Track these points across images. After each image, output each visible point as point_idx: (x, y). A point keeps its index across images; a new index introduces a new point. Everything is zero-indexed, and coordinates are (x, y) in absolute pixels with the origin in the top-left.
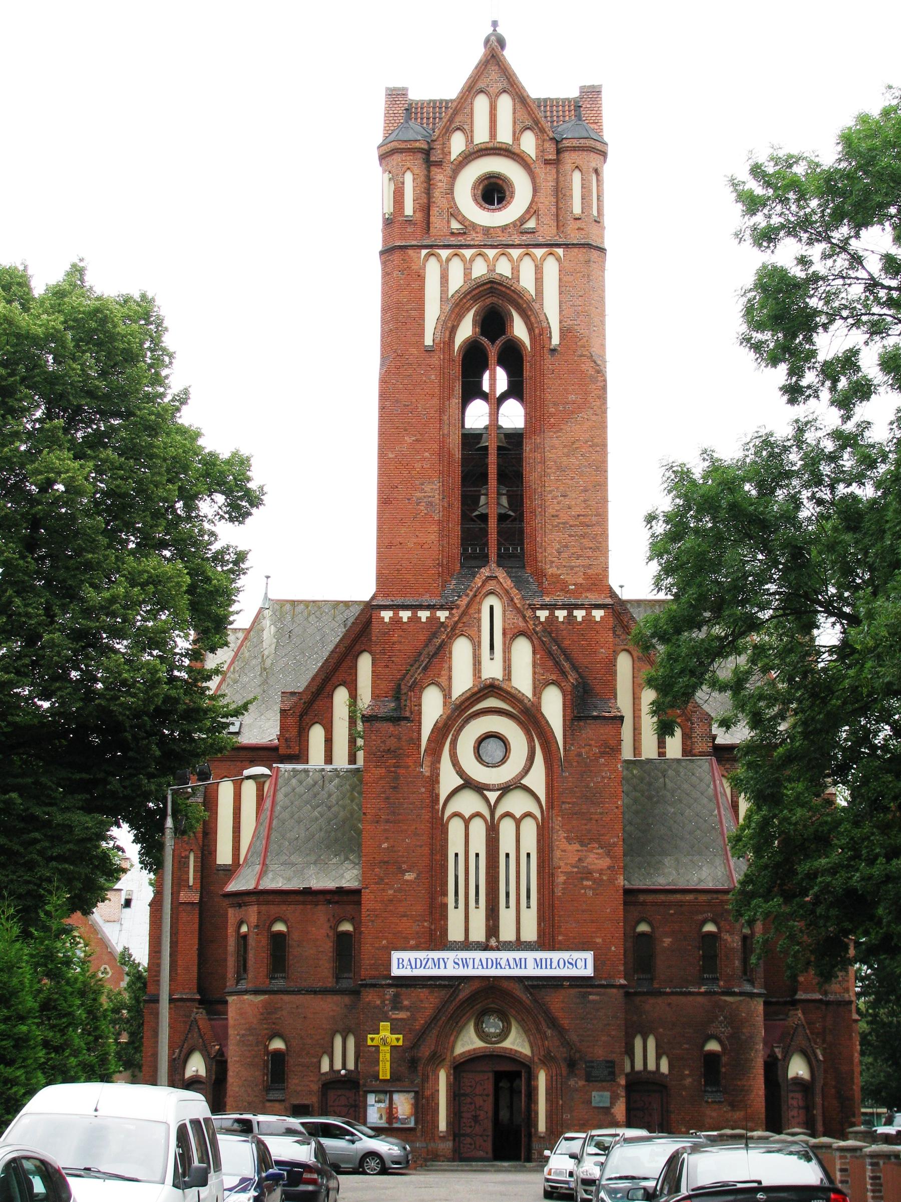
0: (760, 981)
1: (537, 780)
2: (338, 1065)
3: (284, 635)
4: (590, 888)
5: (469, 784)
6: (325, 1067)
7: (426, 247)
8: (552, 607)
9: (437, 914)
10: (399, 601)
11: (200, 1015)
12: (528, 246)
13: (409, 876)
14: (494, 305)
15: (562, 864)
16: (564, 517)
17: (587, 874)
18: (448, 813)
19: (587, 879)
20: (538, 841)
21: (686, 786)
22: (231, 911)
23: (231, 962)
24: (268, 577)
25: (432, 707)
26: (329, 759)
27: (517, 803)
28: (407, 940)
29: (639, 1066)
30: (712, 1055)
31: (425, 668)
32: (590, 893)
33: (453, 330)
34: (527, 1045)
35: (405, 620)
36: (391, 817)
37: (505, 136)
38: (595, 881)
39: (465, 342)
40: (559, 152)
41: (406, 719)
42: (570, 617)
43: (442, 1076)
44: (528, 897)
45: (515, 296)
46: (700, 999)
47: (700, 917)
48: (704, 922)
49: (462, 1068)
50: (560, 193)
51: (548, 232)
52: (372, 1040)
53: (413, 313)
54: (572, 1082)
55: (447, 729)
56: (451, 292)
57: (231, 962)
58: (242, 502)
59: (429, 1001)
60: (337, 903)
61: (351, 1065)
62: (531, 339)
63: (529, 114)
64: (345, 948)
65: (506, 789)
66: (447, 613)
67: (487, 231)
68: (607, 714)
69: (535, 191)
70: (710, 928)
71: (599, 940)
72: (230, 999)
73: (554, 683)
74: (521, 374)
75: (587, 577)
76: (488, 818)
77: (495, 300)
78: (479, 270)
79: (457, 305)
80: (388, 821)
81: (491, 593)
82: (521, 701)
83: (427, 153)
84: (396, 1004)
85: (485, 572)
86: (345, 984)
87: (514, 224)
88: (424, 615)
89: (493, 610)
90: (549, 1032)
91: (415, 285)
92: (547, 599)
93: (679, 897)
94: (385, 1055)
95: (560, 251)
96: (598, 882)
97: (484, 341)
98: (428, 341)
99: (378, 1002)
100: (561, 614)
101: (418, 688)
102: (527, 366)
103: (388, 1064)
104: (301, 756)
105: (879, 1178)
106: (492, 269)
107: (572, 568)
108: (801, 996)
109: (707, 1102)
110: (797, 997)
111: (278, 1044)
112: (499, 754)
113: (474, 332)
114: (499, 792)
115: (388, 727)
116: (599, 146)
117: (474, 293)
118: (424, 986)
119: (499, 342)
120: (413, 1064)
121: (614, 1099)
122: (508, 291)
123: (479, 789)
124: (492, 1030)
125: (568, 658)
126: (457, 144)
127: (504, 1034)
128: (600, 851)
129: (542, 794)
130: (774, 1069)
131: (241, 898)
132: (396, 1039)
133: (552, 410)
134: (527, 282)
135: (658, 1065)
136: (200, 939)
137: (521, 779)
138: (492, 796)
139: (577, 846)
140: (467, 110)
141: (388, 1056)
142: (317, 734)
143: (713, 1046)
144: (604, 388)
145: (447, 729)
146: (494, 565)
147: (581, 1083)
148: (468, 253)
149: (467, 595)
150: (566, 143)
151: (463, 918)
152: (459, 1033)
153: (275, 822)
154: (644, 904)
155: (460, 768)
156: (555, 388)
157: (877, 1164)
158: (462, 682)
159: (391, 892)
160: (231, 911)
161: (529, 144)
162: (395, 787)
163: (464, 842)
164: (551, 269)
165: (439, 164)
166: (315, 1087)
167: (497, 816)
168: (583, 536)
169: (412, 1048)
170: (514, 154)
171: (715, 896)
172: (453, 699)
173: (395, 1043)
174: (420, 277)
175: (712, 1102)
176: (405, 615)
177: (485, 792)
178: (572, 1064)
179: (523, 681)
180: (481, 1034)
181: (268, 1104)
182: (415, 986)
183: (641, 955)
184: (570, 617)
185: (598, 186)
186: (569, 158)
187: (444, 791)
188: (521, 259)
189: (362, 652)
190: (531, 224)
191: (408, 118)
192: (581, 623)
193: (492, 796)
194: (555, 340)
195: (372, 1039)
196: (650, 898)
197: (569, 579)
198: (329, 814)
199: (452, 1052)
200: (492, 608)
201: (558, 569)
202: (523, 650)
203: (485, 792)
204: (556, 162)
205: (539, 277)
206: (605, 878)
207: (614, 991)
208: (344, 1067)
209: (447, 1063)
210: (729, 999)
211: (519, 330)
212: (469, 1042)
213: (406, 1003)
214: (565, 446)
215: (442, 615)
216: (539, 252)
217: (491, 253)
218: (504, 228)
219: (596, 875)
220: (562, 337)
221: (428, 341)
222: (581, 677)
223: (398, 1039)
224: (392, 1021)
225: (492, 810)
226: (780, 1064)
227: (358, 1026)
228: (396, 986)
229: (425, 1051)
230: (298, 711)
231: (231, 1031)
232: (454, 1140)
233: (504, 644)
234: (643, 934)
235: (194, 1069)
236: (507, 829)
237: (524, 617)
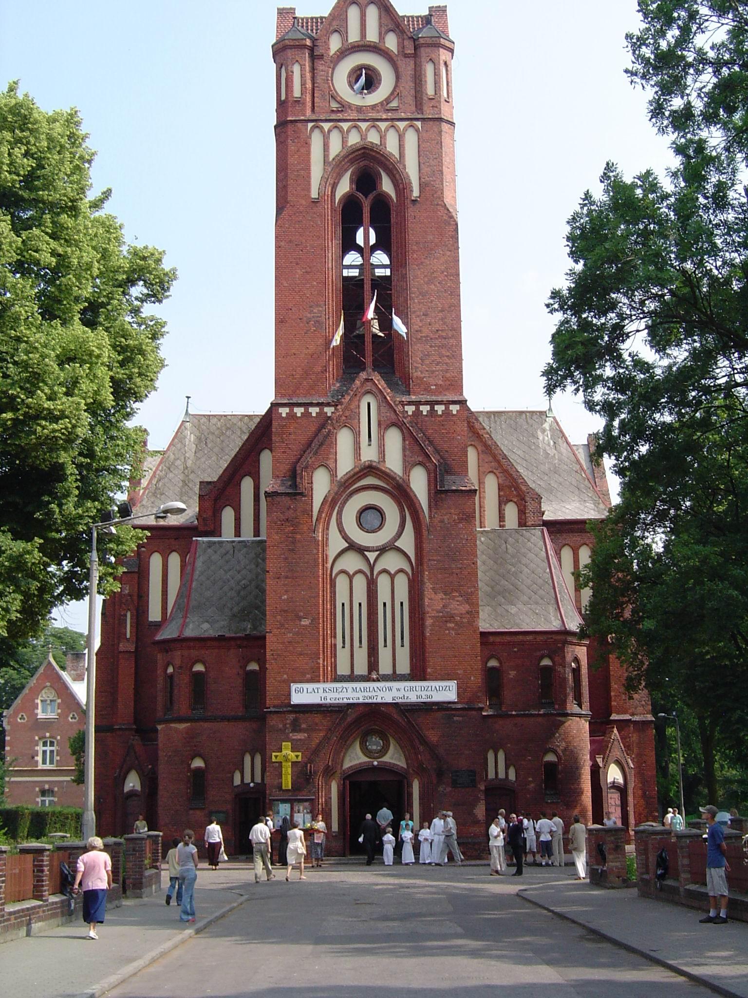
0: (586, 704)
1: (407, 542)
2: (247, 779)
3: (201, 441)
4: (453, 629)
6: (237, 781)
8: (418, 404)
10: (294, 401)
11: (136, 741)
12: (392, 120)
14: (368, 165)
15: (430, 610)
16: (426, 331)
17: (451, 617)
20: (410, 592)
21: (523, 550)
22: (159, 656)
23: (160, 699)
24: (188, 397)
25: (321, 485)
26: (238, 533)
27: (392, 562)
31: (316, 453)
33: (334, 186)
34: (403, 760)
35: (299, 415)
36: (289, 574)
37: (372, 36)
38: (456, 624)
39: (344, 196)
40: (416, 48)
41: (301, 494)
42: (432, 411)
44: (402, 638)
45: (383, 159)
46: (540, 719)
47: (538, 654)
48: (542, 657)
50: (418, 79)
53: (302, 172)
54: (441, 789)
55: (335, 501)
57: (160, 699)
58: (159, 289)
61: (258, 779)
62: (397, 195)
63: (392, 20)
64: (254, 685)
65: (382, 550)
66: (332, 409)
67: (359, 109)
68: (464, 488)
69: (398, 78)
70: (546, 662)
72: (159, 727)
73: (420, 464)
74: (389, 229)
75: (445, 379)
76: (369, 575)
77: (366, 162)
78: (354, 139)
79: (337, 166)
80: (287, 577)
81: (368, 392)
82: (394, 479)
83: (312, 50)
84: (296, 728)
85: (363, 375)
87: (381, 103)
88: (314, 411)
89: (367, 407)
90: (421, 748)
91: (303, 150)
92: (413, 397)
95: (419, 124)
97: (360, 195)
98: (314, 194)
99: (281, 726)
100: (425, 409)
101: (311, 469)
102: (393, 215)
103: (289, 777)
104: (216, 531)
106: (363, 137)
107: (433, 372)
108: (614, 717)
109: (547, 803)
111: (198, 763)
112: (377, 523)
113: (351, 188)
114: (378, 553)
115: (286, 500)
116: (447, 44)
117: (351, 157)
118: (318, 712)
119: (371, 196)
122: (378, 156)
123: (361, 550)
124: (374, 747)
125: (431, 443)
126: (335, 44)
127: (384, 751)
128: (460, 599)
129: (412, 554)
131: (167, 645)
133: (415, 248)
134: (392, 147)
136: (136, 681)
137: (396, 541)
139: (441, 595)
141: (290, 770)
142: (228, 514)
144: (456, 230)
145: (335, 501)
146: (370, 370)
147: (449, 789)
148: (345, 126)
149: (349, 394)
150: (422, 41)
151: (349, 656)
152: (347, 750)
153: (194, 584)
154: (493, 643)
155: (345, 533)
156: (416, 227)
158: (345, 465)
160: (159, 656)
161: (391, 43)
162: (293, 550)
163: (348, 594)
164: (411, 139)
167: (375, 573)
168: (443, 346)
170: (380, 50)
172: (339, 478)
173: (295, 759)
175: (552, 803)
176: (298, 411)
177: (366, 553)
178: (440, 774)
179: (394, 463)
180: (366, 751)
181: (191, 812)
183: (493, 682)
184: (432, 411)
185: (447, 74)
186: (423, 51)
187: (332, 553)
188: (387, 130)
189: (264, 449)
190: (394, 104)
192: (441, 416)
193: (372, 556)
194: (416, 193)
195: (276, 757)
197: (431, 380)
198: (239, 577)
199: (342, 766)
200: (369, 404)
201: (422, 372)
202: (394, 440)
203: (366, 553)
204: (415, 56)
205: (403, 145)
206: (465, 620)
207: (474, 713)
208: (253, 781)
209: (338, 775)
211: (387, 186)
212: (355, 758)
213: (304, 726)
215: (329, 411)
216: (402, 125)
217: (364, 125)
218: (373, 107)
221: (314, 194)
222: (442, 458)
224: (293, 741)
226: (601, 770)
228: (296, 712)
233: (379, 432)
234: (493, 668)
235: (131, 785)
236: (383, 582)
237: (395, 411)
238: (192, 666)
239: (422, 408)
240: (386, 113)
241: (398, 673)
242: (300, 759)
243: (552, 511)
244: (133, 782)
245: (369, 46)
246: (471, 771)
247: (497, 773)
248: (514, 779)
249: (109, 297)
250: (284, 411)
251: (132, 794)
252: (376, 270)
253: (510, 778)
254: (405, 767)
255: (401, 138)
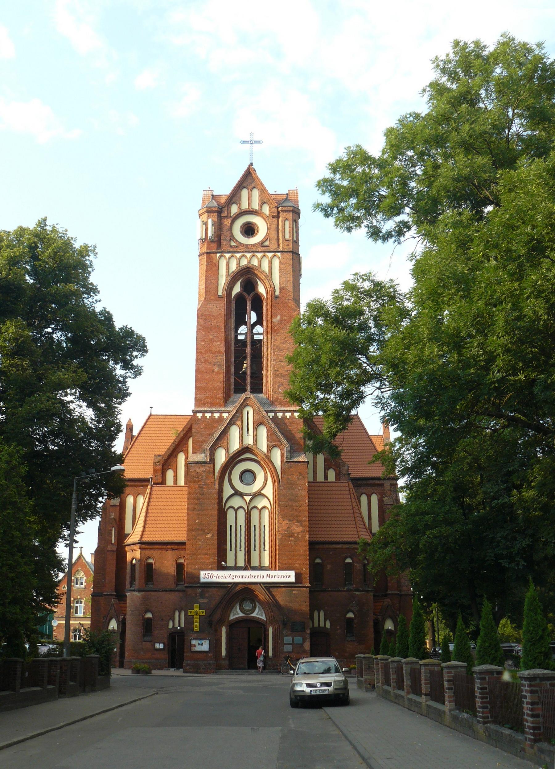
1: (269, 491)
2: (177, 624)
5: (237, 493)
6: (171, 626)
7: (219, 252)
9: (221, 554)
12: (265, 252)
13: (209, 536)
17: (292, 534)
18: (227, 507)
19: (292, 537)
24: (151, 407)
28: (207, 565)
29: (316, 625)
30: (350, 619)
32: (293, 543)
34: (264, 615)
38: (295, 538)
43: (224, 630)
46: (344, 593)
48: (346, 558)
49: (233, 626)
51: (274, 247)
52: (191, 612)
56: (231, 271)
59: (218, 594)
60: (177, 549)
61: (183, 625)
67: (247, 246)
70: (349, 560)
71: (297, 565)
72: (128, 594)
78: (244, 262)
84: (202, 595)
85: (244, 396)
86: (179, 587)
87: (259, 243)
93: (334, 546)
94: (197, 620)
95: (279, 254)
96: (297, 538)
98: (220, 293)
104: (163, 482)
105: (486, 688)
108: (389, 592)
110: (388, 593)
111: (149, 615)
118: (215, 587)
119: (252, 294)
120: (210, 623)
121: (304, 640)
123: (241, 495)
124: (247, 608)
126: (234, 209)
127: (253, 611)
129: (271, 497)
130: (378, 625)
132: (202, 612)
135: (325, 624)
138: (248, 498)
139: (286, 521)
140: (238, 195)
141: (198, 620)
142: (170, 474)
143: (350, 615)
157: (484, 679)
158: (235, 446)
159: (200, 543)
164: (276, 263)
165: (227, 217)
166: (166, 635)
169: (210, 616)
171: (351, 546)
173: (201, 614)
174: (217, 266)
178: (285, 624)
180: (242, 610)
181: (144, 643)
182: (211, 587)
190: (267, 243)
191: (213, 199)
195: (191, 612)
196: (321, 546)
199: (229, 618)
202: (263, 432)
203: (245, 497)
207: (304, 589)
208: (179, 626)
210: (358, 593)
211: (261, 289)
212: (237, 614)
213: (207, 595)
214: (281, 340)
219: (296, 535)
220: (280, 292)
223: (203, 612)
225: (248, 505)
227: (186, 607)
228: (202, 587)
229: (216, 617)
230: (162, 463)
231: (128, 609)
232: (229, 660)
234: (318, 564)
236: (255, 514)
238: (314, 560)
239: (278, 414)
240: (262, 247)
241: (237, 565)
242: (204, 614)
243: (356, 473)
244: (113, 625)
245: (244, 212)
246: (303, 622)
247: (319, 624)
248: (329, 627)
249: (103, 352)
250: (199, 415)
251: (113, 631)
252: (255, 336)
253: (327, 626)
254: (265, 619)
255: (270, 263)
